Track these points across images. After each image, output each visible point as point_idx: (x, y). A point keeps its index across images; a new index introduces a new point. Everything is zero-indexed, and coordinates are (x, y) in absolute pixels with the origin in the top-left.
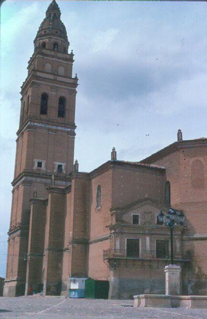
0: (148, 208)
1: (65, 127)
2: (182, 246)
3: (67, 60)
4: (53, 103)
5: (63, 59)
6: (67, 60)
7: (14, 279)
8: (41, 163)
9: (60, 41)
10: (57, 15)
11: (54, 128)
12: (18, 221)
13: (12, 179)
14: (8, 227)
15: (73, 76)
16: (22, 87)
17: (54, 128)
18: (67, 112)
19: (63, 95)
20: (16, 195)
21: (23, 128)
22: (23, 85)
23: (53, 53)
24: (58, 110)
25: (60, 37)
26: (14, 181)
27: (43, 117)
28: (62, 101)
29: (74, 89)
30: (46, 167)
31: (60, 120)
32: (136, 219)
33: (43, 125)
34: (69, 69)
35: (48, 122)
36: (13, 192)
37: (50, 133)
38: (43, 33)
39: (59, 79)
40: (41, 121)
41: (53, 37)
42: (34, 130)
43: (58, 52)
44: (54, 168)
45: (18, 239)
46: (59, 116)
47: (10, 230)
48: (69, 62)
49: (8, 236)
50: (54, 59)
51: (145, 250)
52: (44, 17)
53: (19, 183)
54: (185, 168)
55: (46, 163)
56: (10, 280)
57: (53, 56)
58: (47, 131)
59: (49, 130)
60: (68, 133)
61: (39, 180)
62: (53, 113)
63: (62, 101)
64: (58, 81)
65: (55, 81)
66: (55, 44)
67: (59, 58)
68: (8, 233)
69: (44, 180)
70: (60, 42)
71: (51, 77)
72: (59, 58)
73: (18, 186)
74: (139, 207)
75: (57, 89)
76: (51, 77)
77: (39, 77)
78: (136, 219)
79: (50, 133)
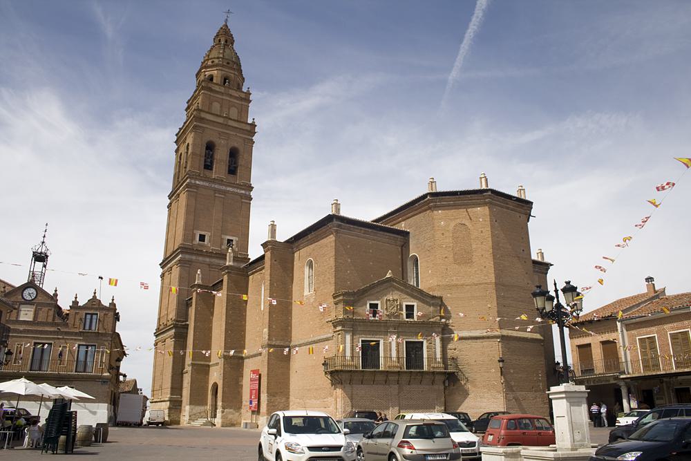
3: (241, 99)
4: (221, 155)
5: (236, 98)
6: (241, 99)
11: (224, 188)
14: (155, 326)
15: (250, 121)
16: (177, 135)
17: (224, 188)
19: (236, 145)
23: (222, 89)
26: (163, 261)
28: (234, 154)
33: (207, 184)
35: (214, 181)
36: (162, 276)
38: (209, 63)
39: (231, 123)
47: (158, 329)
50: (224, 97)
54: (443, 234)
57: (222, 94)
59: (215, 190)
60: (241, 196)
61: (201, 258)
63: (234, 154)
64: (229, 126)
67: (231, 96)
69: (208, 260)
71: (220, 120)
72: (231, 96)
77: (203, 119)
79: (243, 200)
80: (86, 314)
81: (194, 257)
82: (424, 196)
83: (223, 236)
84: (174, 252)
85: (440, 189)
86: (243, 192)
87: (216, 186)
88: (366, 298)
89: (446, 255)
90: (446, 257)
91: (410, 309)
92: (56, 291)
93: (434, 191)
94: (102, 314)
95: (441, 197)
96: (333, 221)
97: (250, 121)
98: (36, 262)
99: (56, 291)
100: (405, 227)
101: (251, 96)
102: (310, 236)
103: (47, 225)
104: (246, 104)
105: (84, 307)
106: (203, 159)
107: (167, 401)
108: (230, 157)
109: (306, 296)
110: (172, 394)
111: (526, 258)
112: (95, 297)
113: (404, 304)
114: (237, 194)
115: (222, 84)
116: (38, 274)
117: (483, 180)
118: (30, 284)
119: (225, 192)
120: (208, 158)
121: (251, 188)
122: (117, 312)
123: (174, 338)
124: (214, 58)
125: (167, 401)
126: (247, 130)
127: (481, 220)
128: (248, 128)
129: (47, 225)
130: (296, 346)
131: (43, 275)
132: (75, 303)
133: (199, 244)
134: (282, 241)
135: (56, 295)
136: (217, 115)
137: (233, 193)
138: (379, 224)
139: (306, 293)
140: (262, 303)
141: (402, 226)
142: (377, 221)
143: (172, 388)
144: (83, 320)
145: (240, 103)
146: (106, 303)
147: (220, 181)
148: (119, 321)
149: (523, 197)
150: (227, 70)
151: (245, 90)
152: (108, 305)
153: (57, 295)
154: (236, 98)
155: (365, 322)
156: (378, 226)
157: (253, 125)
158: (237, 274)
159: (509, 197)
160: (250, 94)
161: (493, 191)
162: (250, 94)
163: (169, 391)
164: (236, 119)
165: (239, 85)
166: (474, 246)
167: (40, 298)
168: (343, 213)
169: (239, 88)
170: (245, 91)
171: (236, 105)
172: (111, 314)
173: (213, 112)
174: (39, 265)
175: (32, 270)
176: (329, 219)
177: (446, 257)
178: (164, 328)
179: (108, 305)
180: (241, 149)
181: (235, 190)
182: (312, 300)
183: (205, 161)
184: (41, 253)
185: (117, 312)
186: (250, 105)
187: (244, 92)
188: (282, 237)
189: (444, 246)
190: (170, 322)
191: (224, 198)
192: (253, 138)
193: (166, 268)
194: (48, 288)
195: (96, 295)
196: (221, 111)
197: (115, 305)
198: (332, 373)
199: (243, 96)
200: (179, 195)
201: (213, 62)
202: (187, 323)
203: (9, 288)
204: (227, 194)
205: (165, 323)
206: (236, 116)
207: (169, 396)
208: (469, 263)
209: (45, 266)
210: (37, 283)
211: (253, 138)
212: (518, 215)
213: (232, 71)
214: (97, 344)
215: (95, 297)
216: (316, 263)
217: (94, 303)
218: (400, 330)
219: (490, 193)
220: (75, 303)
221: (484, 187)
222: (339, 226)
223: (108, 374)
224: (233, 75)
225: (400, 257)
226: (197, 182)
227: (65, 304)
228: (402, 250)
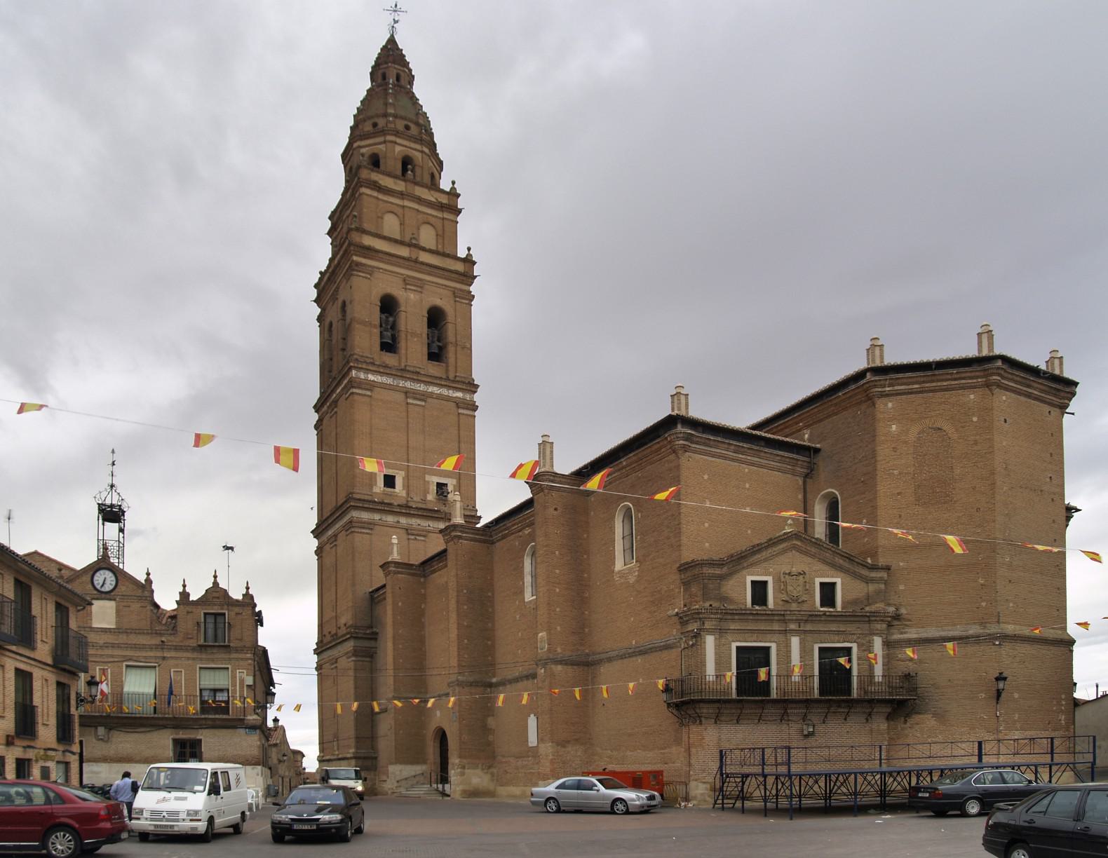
0: (794, 562)
1: (449, 387)
2: (888, 661)
3: (441, 207)
4: (413, 323)
5: (430, 204)
6: (441, 207)
7: (349, 756)
8: (393, 477)
9: (418, 155)
10: (403, 82)
11: (421, 387)
12: (343, 621)
13: (313, 521)
14: (314, 638)
15: (462, 253)
16: (316, 286)
17: (421, 387)
18: (451, 350)
19: (438, 302)
20: (329, 561)
21: (333, 391)
22: (320, 279)
23: (400, 186)
24: (426, 341)
25: (419, 140)
26: (318, 525)
27: (389, 359)
28: (435, 318)
29: (464, 287)
30: (407, 486)
31: (434, 369)
32: (759, 590)
33: (389, 381)
34: (448, 234)
35: (403, 373)
36: (319, 552)
37: (410, 401)
38: (368, 127)
39: (425, 257)
40: (384, 370)
41: (399, 140)
42: (368, 393)
43: (416, 184)
44: (426, 492)
45: (347, 663)
46: (429, 359)
47: (319, 643)
48: (446, 215)
49: (315, 658)
50: (407, 203)
51: (786, 674)
52: (368, 84)
53: (337, 526)
54: (895, 449)
55: (407, 479)
56: (335, 757)
57: (401, 195)
58: (403, 396)
59: (407, 393)
60: (459, 404)
61: (390, 519)
62: (414, 347)
63: (435, 318)
64: (422, 263)
65: (414, 263)
66: (406, 162)
67: (420, 200)
68: (315, 650)
69: (403, 520)
70: (417, 156)
71: (404, 252)
72: (420, 200)
73: (335, 536)
74: (766, 560)
75: (420, 286)
76: (404, 252)
77: (369, 249)
78: (759, 590)
80: (205, 614)
81: (377, 517)
82: (859, 376)
83: (428, 478)
84: (337, 509)
85: (891, 359)
86: (459, 394)
87: (408, 384)
88: (744, 572)
89: (899, 491)
90: (899, 494)
91: (828, 590)
92: (148, 574)
93: (878, 363)
94: (233, 614)
95: (893, 376)
96: (676, 428)
97: (462, 253)
98: (106, 523)
99: (148, 574)
100: (809, 440)
101: (460, 200)
102: (624, 461)
103: (113, 452)
104: (451, 217)
105: (202, 601)
106: (377, 331)
107: (351, 758)
108: (429, 327)
109: (620, 571)
110: (357, 748)
111: (1054, 494)
112: (216, 584)
113: (818, 581)
114: (448, 399)
115: (399, 172)
116: (112, 545)
117: (985, 338)
118: (103, 563)
119: (424, 396)
120: (386, 330)
121: (472, 387)
122: (257, 610)
123: (354, 655)
124: (378, 116)
125: (351, 758)
126: (456, 272)
127: (975, 419)
128: (460, 267)
129: (113, 452)
130: (503, 683)
131: (121, 547)
132: (184, 595)
133: (385, 494)
134: (567, 474)
135: (149, 581)
136: (396, 241)
137: (440, 397)
138: (758, 433)
139: (619, 565)
140: (183, 686)
141: (805, 438)
142: (755, 427)
143: (357, 738)
144: (202, 625)
145: (440, 214)
146: (237, 594)
147: (416, 376)
148: (262, 625)
149: (1057, 372)
150: (405, 143)
151: (445, 185)
152: (240, 598)
153: (151, 582)
154: (430, 204)
155: (742, 614)
156: (756, 436)
157: (469, 261)
158: (472, 540)
159: (1034, 371)
160: (458, 196)
161: (1005, 359)
162: (458, 196)
163: (352, 742)
164: (434, 248)
165: (433, 176)
166: (957, 471)
167: (123, 588)
168: (695, 412)
169: (434, 184)
170: (448, 189)
171: (432, 220)
172: (248, 611)
173: (386, 234)
174: (112, 528)
175: (101, 538)
176: (669, 423)
177: (899, 494)
178: (330, 642)
179: (240, 598)
180: (450, 317)
181: (445, 392)
182: (632, 580)
183: (382, 336)
184: (112, 506)
185: (257, 610)
186: (459, 219)
187: (443, 192)
188: (565, 464)
189: (896, 472)
190: (343, 631)
191: (423, 406)
192: (472, 288)
193: (324, 538)
194: (135, 568)
195: (218, 580)
196: (402, 231)
197: (252, 597)
198: (678, 706)
199: (444, 200)
200: (335, 402)
201: (375, 125)
202: (374, 630)
203: (67, 572)
204: (429, 400)
205: (333, 632)
206: (434, 242)
207: (352, 750)
208: (945, 503)
209: (121, 530)
210: (114, 561)
211: (472, 288)
212: (1046, 408)
213: (418, 147)
214: (229, 666)
215: (216, 584)
216: (639, 511)
217: (216, 594)
218: (809, 627)
219: (999, 363)
220: (184, 595)
221: (985, 353)
222: (688, 438)
223: (255, 717)
224: (418, 155)
225: (800, 496)
226: (371, 377)
227: (167, 600)
228: (805, 483)
